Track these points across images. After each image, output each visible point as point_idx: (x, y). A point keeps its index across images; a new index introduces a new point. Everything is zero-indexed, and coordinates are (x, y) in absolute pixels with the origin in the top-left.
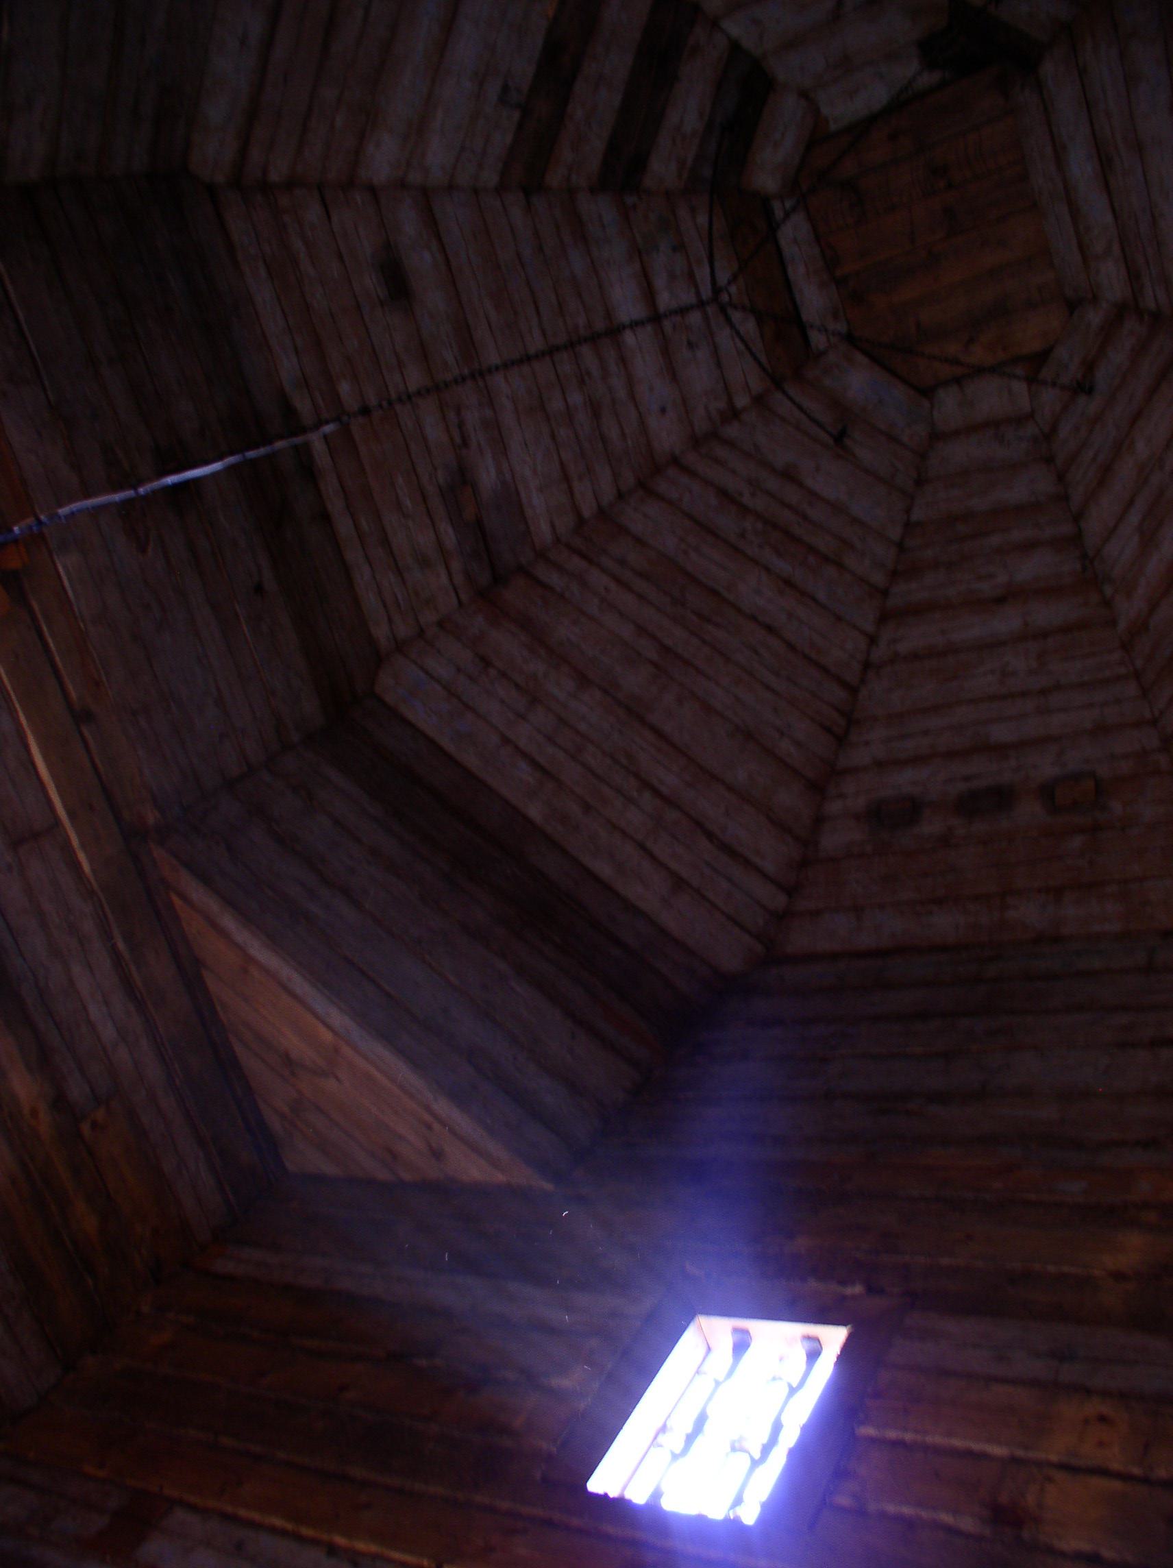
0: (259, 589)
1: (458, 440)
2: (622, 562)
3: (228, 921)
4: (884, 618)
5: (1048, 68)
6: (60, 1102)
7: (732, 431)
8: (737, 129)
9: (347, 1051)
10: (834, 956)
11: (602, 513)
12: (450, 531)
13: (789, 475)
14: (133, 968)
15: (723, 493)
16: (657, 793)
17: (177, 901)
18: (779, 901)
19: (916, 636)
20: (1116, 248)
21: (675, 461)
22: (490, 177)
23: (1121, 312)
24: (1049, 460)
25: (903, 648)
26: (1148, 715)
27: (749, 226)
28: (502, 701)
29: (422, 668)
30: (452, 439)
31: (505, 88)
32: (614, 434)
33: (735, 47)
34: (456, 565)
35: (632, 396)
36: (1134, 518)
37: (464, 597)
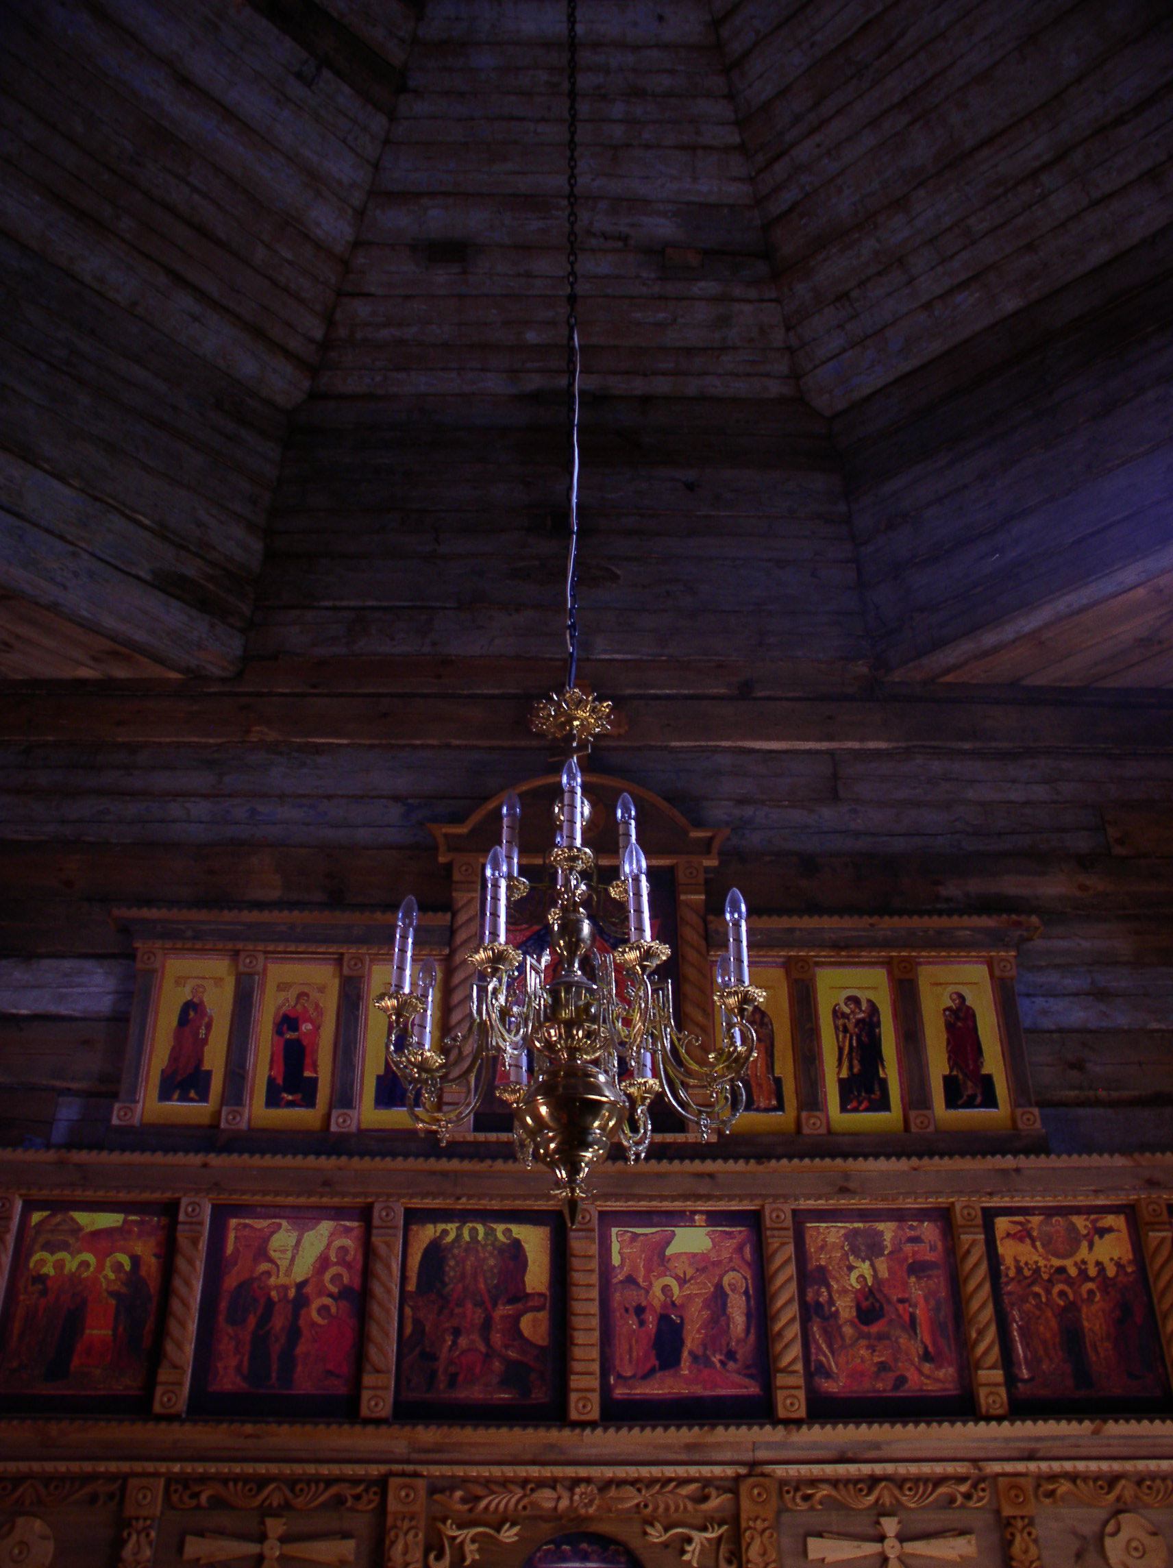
0: (690, 487)
1: (620, 244)
3: (989, 639)
6: (1084, 862)
9: (1162, 581)
12: (702, 284)
14: (993, 744)
16: (1046, 167)
17: (948, 678)
21: (716, 23)
22: (378, 123)
28: (889, 294)
29: (824, 363)
31: (299, 76)
34: (738, 291)
35: (635, 48)
37: (773, 295)
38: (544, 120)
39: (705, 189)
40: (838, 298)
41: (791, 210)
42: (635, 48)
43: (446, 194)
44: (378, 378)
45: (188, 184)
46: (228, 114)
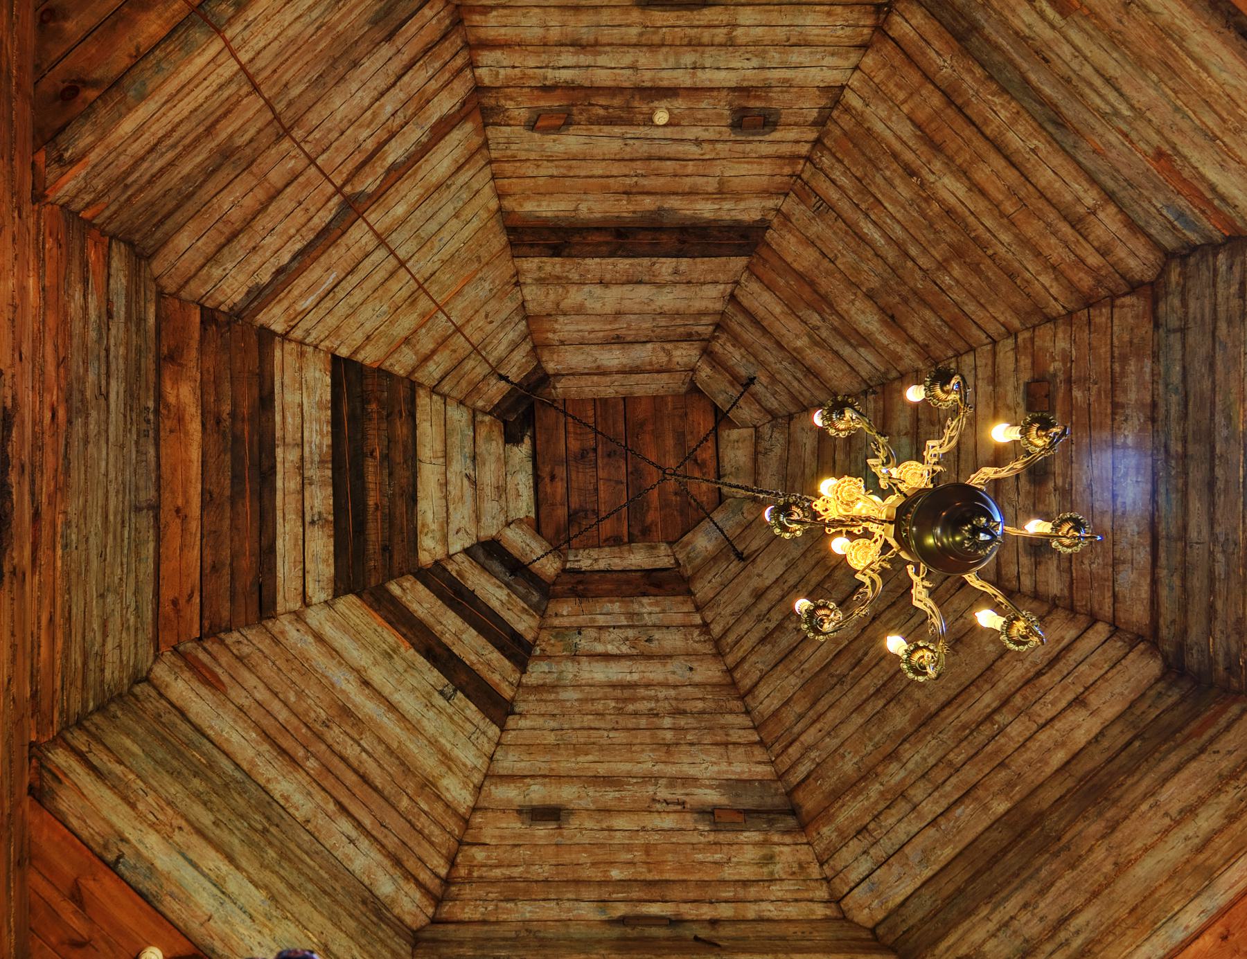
1: (679, 807)
2: (801, 717)
5: (551, 367)
7: (717, 629)
8: (515, 569)
10: (1154, 582)
15: (762, 641)
16: (996, 710)
18: (1102, 629)
20: (669, 346)
22: (493, 730)
23: (707, 353)
24: (790, 417)
26: (989, 347)
27: (581, 586)
28: (900, 821)
29: (858, 885)
30: (675, 812)
31: (441, 693)
32: (700, 705)
33: (466, 551)
35: (675, 687)
36: (846, 351)
38: (614, 729)
39: (739, 770)
40: (859, 832)
42: (675, 687)
43: (545, 776)
45: (359, 745)
46: (392, 707)
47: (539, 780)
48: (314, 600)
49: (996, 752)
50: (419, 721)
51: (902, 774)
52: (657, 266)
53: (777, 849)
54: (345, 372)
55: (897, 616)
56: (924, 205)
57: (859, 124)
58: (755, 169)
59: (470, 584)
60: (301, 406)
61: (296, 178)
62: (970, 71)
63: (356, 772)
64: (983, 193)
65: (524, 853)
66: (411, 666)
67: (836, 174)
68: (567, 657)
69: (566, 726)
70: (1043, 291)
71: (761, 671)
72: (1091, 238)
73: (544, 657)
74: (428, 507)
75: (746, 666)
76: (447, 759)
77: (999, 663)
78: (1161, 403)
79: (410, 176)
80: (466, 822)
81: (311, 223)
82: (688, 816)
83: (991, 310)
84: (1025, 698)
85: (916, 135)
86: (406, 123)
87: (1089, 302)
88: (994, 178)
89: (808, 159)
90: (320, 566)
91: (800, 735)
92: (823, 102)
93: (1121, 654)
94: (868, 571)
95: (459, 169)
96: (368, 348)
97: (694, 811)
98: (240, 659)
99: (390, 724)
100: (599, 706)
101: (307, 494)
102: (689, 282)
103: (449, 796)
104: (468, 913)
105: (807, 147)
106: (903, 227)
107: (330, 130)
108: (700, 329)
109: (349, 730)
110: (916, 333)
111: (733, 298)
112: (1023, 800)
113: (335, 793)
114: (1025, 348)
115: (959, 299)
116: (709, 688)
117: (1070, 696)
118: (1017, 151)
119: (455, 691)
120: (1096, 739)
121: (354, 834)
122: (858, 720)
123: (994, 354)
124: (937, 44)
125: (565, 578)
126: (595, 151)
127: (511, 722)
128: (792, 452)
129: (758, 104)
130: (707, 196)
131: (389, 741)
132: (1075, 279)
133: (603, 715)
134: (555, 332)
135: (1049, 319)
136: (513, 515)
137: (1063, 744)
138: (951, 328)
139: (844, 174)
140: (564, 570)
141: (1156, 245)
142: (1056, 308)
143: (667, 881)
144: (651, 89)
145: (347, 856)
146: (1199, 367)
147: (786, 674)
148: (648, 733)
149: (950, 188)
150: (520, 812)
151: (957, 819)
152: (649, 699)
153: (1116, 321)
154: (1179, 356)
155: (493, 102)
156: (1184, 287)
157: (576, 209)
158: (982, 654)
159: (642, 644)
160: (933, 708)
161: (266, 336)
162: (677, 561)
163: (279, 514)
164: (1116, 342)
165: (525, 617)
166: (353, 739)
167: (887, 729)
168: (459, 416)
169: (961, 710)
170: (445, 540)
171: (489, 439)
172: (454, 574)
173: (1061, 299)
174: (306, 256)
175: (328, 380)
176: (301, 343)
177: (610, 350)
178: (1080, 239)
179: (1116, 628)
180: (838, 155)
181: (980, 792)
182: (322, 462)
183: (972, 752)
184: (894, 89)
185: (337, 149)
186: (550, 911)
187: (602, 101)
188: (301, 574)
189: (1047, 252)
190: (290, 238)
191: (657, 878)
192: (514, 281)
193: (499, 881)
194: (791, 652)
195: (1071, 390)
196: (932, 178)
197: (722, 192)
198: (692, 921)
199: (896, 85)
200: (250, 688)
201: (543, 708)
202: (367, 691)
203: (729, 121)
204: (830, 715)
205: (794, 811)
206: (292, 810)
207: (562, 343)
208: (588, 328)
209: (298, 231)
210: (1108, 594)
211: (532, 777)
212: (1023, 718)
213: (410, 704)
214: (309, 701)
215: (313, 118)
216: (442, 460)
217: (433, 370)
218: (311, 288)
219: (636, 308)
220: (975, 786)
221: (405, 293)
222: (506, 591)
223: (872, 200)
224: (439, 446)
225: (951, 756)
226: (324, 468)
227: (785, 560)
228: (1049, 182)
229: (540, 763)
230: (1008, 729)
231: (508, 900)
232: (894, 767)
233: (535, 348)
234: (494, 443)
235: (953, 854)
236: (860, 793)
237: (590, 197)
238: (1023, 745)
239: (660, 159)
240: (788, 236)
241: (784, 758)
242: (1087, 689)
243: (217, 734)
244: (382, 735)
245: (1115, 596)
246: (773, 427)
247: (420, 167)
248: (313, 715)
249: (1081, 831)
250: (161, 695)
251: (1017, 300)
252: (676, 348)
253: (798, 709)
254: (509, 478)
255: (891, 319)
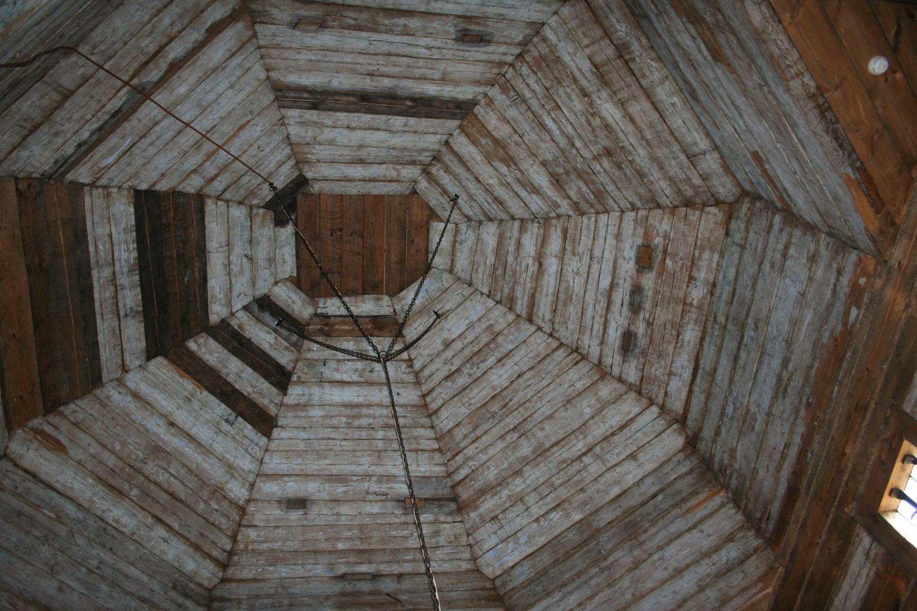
1: (384, 497)
2: (465, 436)
4: (530, 320)
5: (309, 175)
7: (417, 365)
8: (285, 320)
10: (690, 391)
11: (437, 439)
13: (447, 344)
15: (447, 378)
16: (584, 454)
18: (655, 409)
19: (544, 309)
22: (263, 440)
23: (426, 172)
24: (480, 222)
25: (548, 316)
26: (618, 214)
27: (326, 327)
30: (381, 501)
31: (227, 421)
33: (246, 308)
36: (523, 194)
39: (423, 469)
40: (492, 519)
41: (466, 478)
43: (297, 475)
44: (260, 570)
45: (168, 472)
46: (191, 438)
47: (293, 478)
48: (131, 367)
49: (580, 481)
50: (211, 445)
51: (523, 486)
52: (391, 121)
53: (443, 526)
54: (147, 202)
55: (534, 377)
56: (590, 117)
57: (551, 51)
58: (471, 68)
59: (247, 334)
60: (110, 236)
61: (87, 80)
62: (638, 39)
63: (166, 491)
64: (632, 120)
65: (282, 532)
66: (204, 405)
67: (531, 81)
68: (315, 383)
69: (312, 437)
70: (660, 191)
71: (444, 399)
72: (698, 168)
73: (300, 382)
74: (216, 283)
75: (434, 394)
76: (231, 469)
77: (591, 422)
78: (719, 286)
79: (190, 65)
80: (242, 510)
81: (104, 109)
82: (389, 504)
83: (624, 192)
84: (602, 449)
85: (592, 71)
86: (184, 29)
87: (689, 204)
88: (642, 114)
89: (511, 65)
90: (134, 344)
91: (464, 449)
92: (527, 32)
93: (662, 429)
94: (806, 110)
95: (233, 55)
96: (163, 181)
97: (392, 500)
98: (76, 425)
99: (189, 451)
100: (335, 421)
101: (120, 297)
102: (415, 132)
103: (231, 494)
104: (246, 574)
105: (512, 58)
106: (573, 127)
107: (114, 43)
108: (422, 158)
109: (160, 463)
110: (573, 193)
111: (447, 143)
112: (590, 515)
113: (152, 510)
114: (642, 222)
115: (604, 181)
116: (409, 409)
117: (628, 452)
118: (661, 101)
119: (236, 417)
120: (638, 484)
121: (167, 536)
122: (500, 445)
123: (621, 220)
124: (617, 14)
125: (316, 320)
126: (346, 46)
127: (276, 432)
128: (479, 247)
129: (477, 28)
130: (432, 80)
131: (189, 464)
132: (682, 189)
133: (337, 428)
134: (312, 154)
135: (659, 206)
136: (280, 276)
137: (619, 482)
138: (595, 196)
139: (537, 82)
140: (316, 315)
141: (738, 184)
142: (665, 201)
143: (373, 550)
144: (392, 10)
145: (162, 551)
146: (746, 280)
147: (459, 405)
148: (367, 442)
149: (610, 111)
150: (279, 502)
151: (551, 520)
152: (369, 416)
153: (702, 222)
154: (736, 262)
155: (260, 8)
156: (749, 219)
157: (329, 82)
158: (581, 414)
159: (367, 375)
160: (547, 445)
161: (78, 188)
162: (395, 310)
163: (98, 317)
164: (700, 237)
165: (287, 353)
166: (164, 469)
167: (518, 454)
168: (238, 213)
169: (564, 449)
170: (229, 303)
171: (262, 226)
172: (236, 327)
173: (671, 198)
174: (103, 132)
175: (132, 210)
176: (105, 187)
177: (355, 167)
178: (692, 167)
179: (662, 408)
180: (534, 68)
181: (566, 505)
182: (130, 271)
183: (566, 479)
184: (581, 36)
185: (122, 56)
186: (299, 571)
187: (352, 14)
188: (120, 352)
189: (667, 168)
190: (88, 121)
191: (366, 548)
192: (281, 122)
193: (265, 552)
194: (464, 389)
195: (665, 259)
196: (599, 102)
197: (444, 79)
198: (387, 575)
199: (583, 33)
200: (85, 447)
201: (297, 422)
202: (173, 430)
203: (454, 37)
204: (484, 438)
205: (455, 499)
206: (122, 529)
207: (318, 161)
208: (339, 153)
209: (93, 116)
210: (662, 391)
211: (289, 475)
212: (599, 462)
213: (203, 433)
214: (131, 447)
215: (96, 36)
216: (226, 248)
217: (218, 186)
218: (110, 152)
219: (375, 144)
220: (564, 501)
221: (191, 142)
222: (274, 335)
223: (554, 104)
224: (223, 239)
225: (553, 479)
226: (132, 275)
227: (467, 322)
228: (679, 127)
229: (296, 465)
230: (589, 467)
231: (270, 565)
232: (518, 481)
233: (297, 163)
234: (266, 229)
235: (545, 542)
236: (496, 494)
237: (340, 75)
238: (596, 479)
239: (398, 55)
240: (491, 113)
241: (452, 462)
242: (639, 448)
243: (63, 485)
244: (185, 461)
245: (666, 394)
246: (468, 226)
247: (198, 58)
248: (134, 457)
249: (619, 559)
250: (16, 465)
251: (642, 191)
252: (404, 168)
253: (464, 431)
254: (278, 251)
255: (557, 181)
